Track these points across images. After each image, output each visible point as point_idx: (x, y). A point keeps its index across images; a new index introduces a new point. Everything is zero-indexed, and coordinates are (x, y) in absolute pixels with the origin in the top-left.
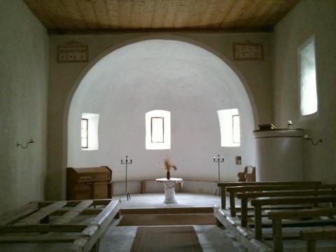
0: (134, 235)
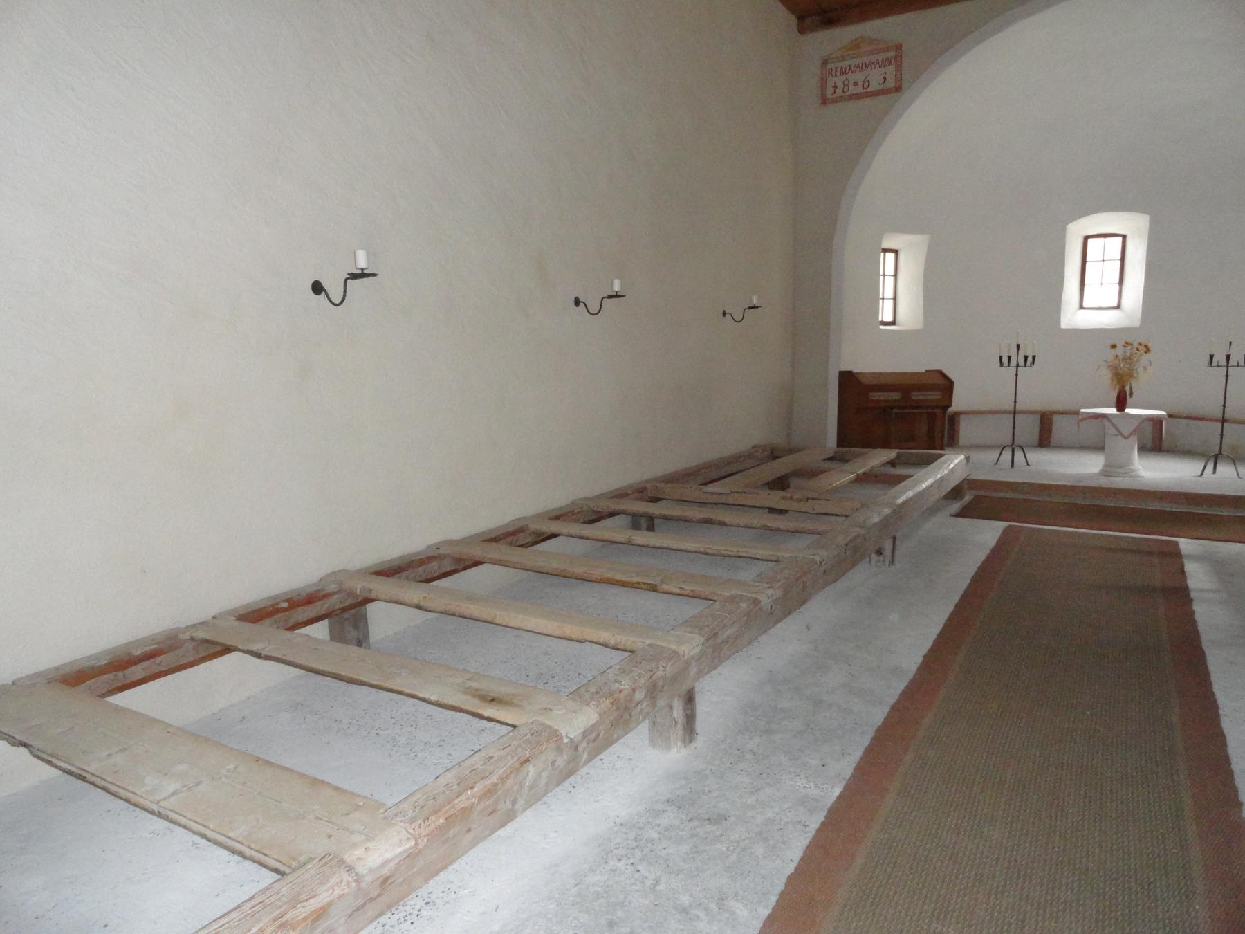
0: (992, 542)
